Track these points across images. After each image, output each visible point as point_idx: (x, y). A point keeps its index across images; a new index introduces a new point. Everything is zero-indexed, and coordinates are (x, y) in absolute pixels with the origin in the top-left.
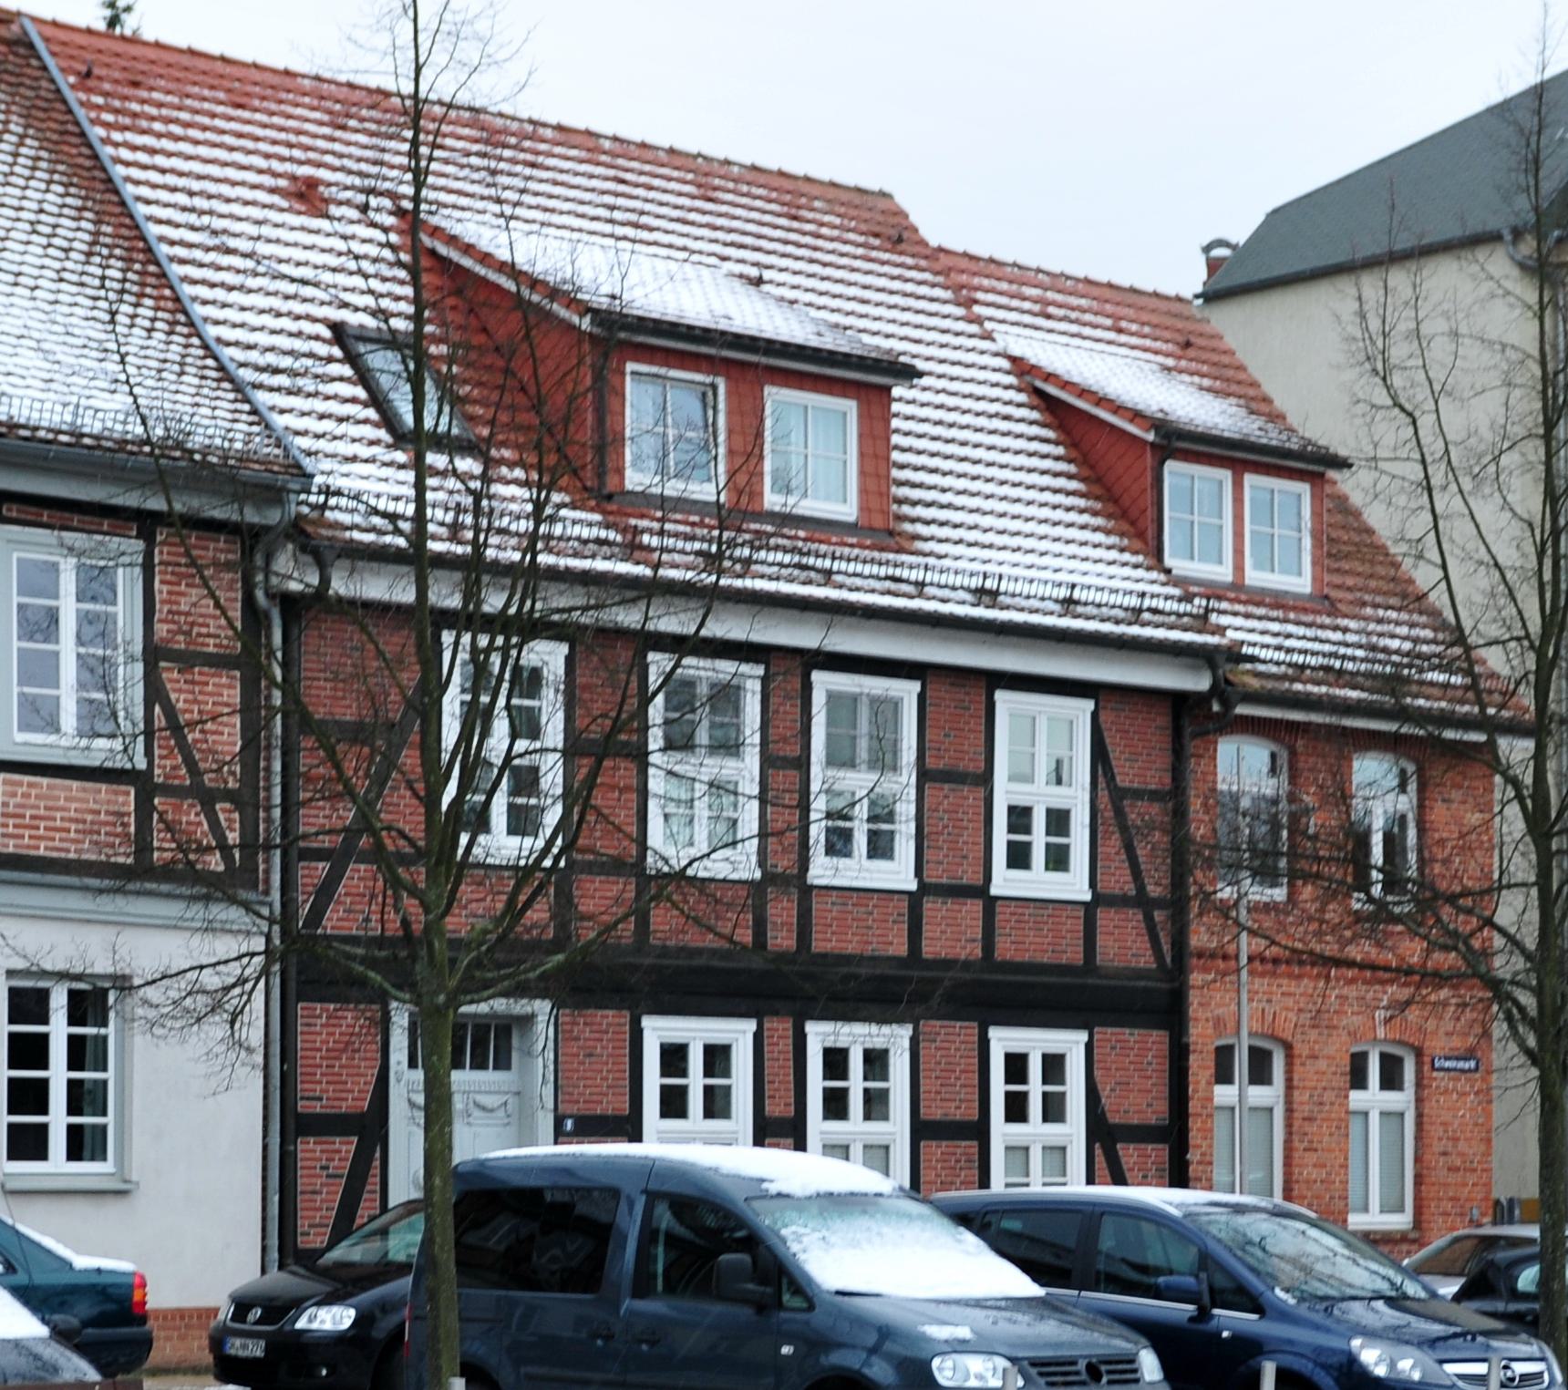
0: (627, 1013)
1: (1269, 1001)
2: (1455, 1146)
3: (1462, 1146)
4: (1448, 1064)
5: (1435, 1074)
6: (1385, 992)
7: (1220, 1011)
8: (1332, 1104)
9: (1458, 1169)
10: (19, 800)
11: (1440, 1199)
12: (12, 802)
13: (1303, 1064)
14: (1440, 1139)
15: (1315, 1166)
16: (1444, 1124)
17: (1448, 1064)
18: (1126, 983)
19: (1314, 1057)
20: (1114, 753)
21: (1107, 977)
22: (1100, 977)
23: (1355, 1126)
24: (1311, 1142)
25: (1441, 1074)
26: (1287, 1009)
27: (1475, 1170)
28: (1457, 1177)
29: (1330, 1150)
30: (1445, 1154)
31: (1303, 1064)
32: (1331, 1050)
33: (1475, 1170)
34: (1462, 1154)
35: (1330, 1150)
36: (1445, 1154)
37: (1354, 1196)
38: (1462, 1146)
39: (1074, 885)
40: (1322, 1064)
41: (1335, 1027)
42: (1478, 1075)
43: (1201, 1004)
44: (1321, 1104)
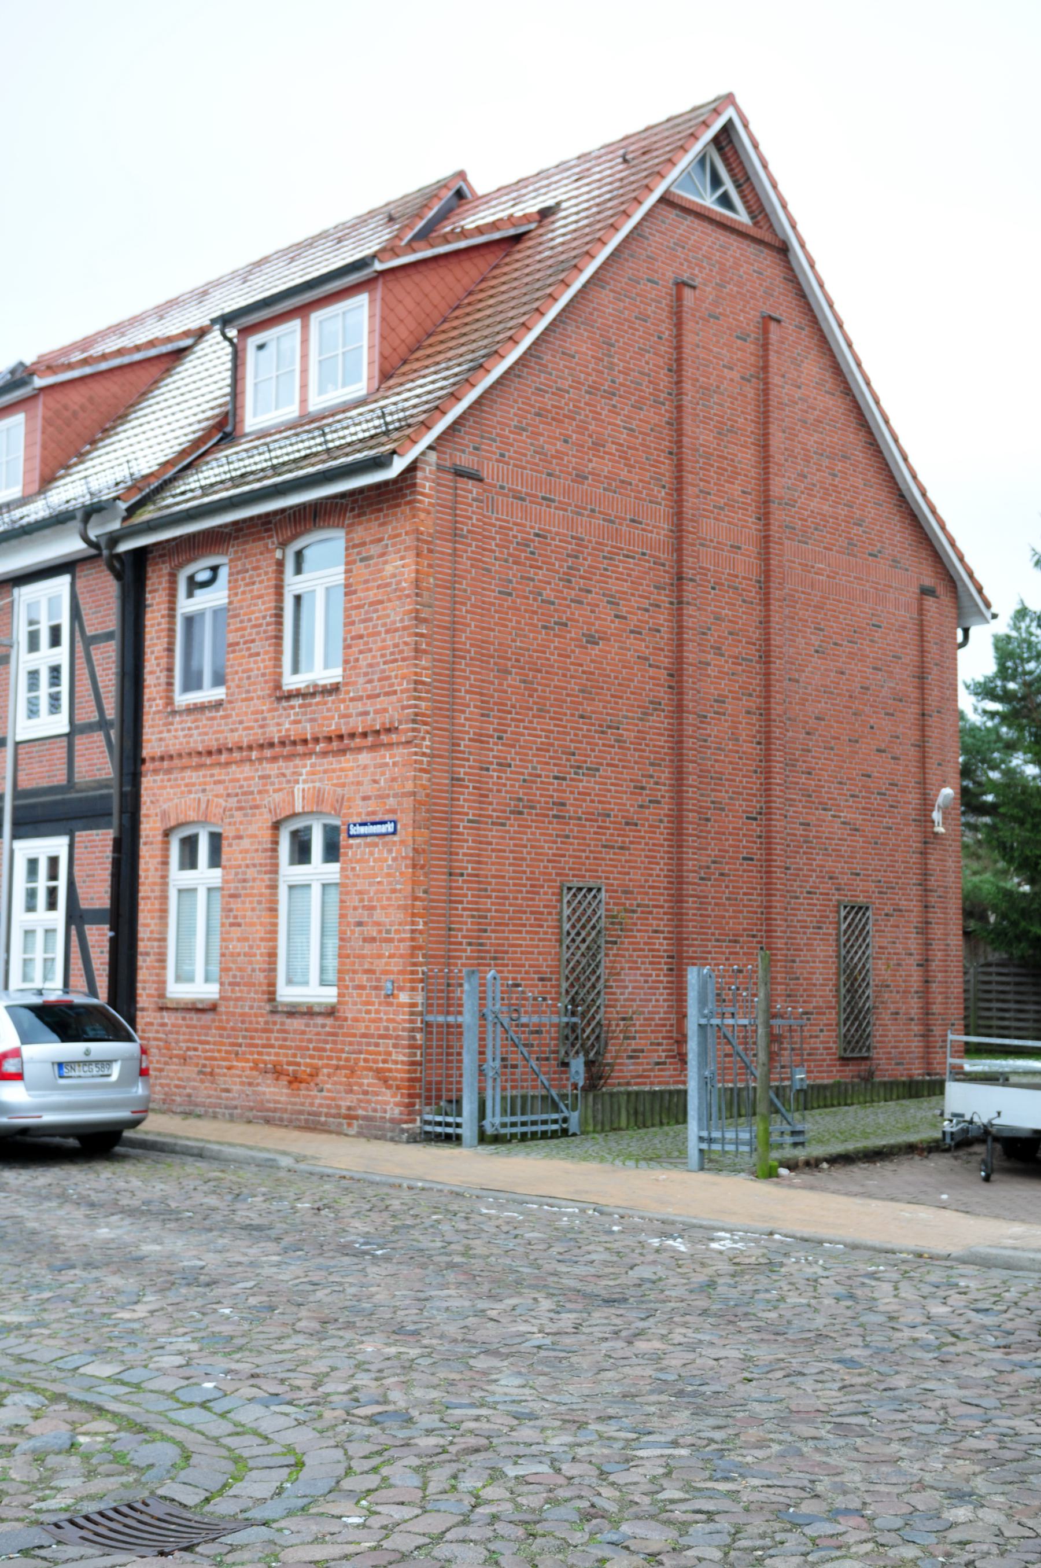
0: (102, 733)
1: (204, 791)
2: (371, 916)
3: (378, 915)
4: (363, 830)
5: (351, 841)
6: (305, 766)
7: (165, 806)
8: (254, 880)
9: (373, 940)
10: (239, 597)
11: (354, 972)
12: (235, 599)
13: (230, 845)
14: (355, 908)
15: (239, 940)
16: (359, 892)
17: (363, 830)
18: (91, 793)
19: (240, 837)
20: (85, 610)
21: (82, 791)
22: (78, 791)
23: (215, 969)
24: (236, 917)
25: (358, 841)
26: (217, 796)
27: (390, 940)
28: (368, 949)
29: (252, 924)
30: (360, 924)
31: (230, 845)
32: (253, 829)
33: (390, 940)
34: (378, 924)
35: (252, 924)
36: (360, 924)
37: (334, 896)
38: (378, 915)
39: (60, 724)
40: (246, 843)
41: (257, 807)
42: (396, 838)
43: (152, 802)
44: (245, 881)
